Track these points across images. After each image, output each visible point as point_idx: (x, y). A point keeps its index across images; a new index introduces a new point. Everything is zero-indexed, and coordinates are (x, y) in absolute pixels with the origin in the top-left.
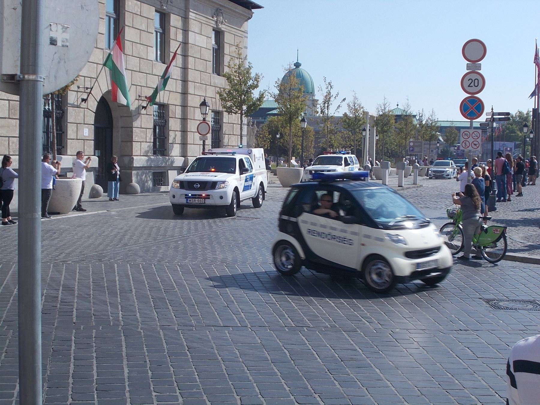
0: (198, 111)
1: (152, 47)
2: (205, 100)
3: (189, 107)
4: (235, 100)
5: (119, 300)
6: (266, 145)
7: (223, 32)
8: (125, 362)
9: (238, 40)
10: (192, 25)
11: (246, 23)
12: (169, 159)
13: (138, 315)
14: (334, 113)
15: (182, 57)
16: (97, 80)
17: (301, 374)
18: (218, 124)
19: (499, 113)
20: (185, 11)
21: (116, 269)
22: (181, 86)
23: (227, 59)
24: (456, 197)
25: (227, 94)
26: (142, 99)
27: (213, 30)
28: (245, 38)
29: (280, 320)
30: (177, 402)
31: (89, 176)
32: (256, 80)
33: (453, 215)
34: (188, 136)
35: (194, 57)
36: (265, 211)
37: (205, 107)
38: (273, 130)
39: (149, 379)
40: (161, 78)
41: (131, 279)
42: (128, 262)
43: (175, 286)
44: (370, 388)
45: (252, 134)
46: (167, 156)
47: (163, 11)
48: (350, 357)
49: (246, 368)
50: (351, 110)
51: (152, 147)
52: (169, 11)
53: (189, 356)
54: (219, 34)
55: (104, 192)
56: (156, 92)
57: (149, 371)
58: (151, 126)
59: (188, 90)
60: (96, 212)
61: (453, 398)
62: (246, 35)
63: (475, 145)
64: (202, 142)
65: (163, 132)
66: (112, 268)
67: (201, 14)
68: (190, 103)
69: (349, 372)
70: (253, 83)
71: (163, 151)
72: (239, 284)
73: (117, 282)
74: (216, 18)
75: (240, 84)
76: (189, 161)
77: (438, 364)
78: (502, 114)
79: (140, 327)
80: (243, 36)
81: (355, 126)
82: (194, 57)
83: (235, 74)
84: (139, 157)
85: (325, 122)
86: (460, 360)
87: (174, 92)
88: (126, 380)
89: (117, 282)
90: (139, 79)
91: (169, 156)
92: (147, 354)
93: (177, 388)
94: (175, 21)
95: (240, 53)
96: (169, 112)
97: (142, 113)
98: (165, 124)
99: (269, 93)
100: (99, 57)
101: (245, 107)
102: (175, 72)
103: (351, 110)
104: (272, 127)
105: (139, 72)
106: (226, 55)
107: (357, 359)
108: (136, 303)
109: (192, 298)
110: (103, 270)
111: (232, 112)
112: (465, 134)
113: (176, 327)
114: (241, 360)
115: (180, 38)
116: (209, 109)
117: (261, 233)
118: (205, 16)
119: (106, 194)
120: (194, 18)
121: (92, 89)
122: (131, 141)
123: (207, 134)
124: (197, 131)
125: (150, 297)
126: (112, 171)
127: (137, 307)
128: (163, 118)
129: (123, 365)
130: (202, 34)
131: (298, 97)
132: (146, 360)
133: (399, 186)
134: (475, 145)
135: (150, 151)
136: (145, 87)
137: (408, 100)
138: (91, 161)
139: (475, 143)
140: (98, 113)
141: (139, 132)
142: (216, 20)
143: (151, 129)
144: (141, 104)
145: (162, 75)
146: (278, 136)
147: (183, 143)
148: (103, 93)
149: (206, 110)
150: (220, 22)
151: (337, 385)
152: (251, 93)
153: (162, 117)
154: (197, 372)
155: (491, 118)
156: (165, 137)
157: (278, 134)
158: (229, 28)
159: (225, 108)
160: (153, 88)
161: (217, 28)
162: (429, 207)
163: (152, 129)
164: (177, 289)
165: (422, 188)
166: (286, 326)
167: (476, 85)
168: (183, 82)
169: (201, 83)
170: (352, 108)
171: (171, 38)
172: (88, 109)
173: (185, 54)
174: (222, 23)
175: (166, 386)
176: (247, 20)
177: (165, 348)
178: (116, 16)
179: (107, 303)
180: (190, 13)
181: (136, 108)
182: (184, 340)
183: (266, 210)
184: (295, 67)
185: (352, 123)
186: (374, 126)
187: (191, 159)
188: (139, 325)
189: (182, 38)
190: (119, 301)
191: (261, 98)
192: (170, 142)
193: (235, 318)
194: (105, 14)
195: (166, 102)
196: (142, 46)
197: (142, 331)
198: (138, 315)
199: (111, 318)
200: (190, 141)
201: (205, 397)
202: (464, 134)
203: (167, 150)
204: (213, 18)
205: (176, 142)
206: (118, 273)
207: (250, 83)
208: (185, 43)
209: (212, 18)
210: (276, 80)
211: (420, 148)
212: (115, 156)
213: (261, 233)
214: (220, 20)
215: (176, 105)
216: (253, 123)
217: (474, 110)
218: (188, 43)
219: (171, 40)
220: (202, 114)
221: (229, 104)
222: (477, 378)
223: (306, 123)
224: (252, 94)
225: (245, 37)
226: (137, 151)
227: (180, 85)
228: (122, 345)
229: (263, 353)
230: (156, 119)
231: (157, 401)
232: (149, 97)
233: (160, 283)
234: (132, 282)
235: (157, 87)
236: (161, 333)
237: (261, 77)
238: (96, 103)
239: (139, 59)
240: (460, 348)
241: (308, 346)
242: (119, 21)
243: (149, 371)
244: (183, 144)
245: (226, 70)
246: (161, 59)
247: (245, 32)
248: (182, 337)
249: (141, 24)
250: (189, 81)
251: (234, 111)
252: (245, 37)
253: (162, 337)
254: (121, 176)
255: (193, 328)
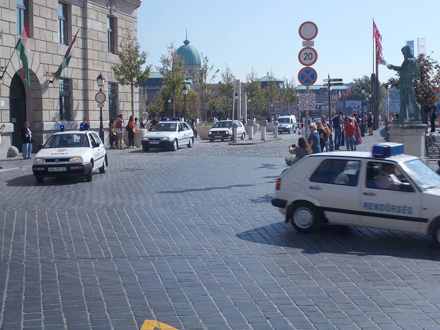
0: (96, 83)
1: (57, 32)
2: (101, 74)
3: (89, 80)
4: (126, 73)
5: (12, 240)
6: (161, 109)
7: (116, 18)
8: (6, 290)
9: (128, 24)
10: (90, 14)
11: (135, 10)
12: (73, 123)
13: (25, 252)
14: (210, 82)
15: (82, 40)
16: (10, 60)
17: (143, 294)
18: (115, 93)
19: (334, 79)
20: (84, 2)
21: (16, 215)
22: (82, 63)
23: (119, 40)
24: (291, 149)
25: (120, 69)
26: (49, 75)
27: (108, 17)
28: (135, 23)
29: (138, 252)
30: (40, 319)
31: (6, 139)
32: (143, 57)
33: (290, 162)
34: (89, 104)
35: (92, 39)
36: (149, 164)
37: (101, 80)
38: (166, 96)
39: (22, 302)
40: (64, 58)
41: (26, 223)
42: (26, 209)
43: (60, 228)
44: (195, 302)
45: (144, 100)
46: (71, 121)
47: (66, 3)
48: (186, 278)
49: (101, 291)
50: (225, 79)
51: (59, 114)
52: (70, 3)
53: (58, 283)
54: (113, 20)
55: (19, 152)
56: (61, 69)
57: (23, 296)
58: (58, 96)
59: (88, 66)
60: (11, 169)
61: (259, 307)
62: (136, 20)
63: (311, 106)
64: (99, 109)
65: (68, 101)
66: (13, 214)
67: (97, 4)
68: (90, 77)
69: (183, 290)
70: (141, 60)
71: (69, 117)
72: (276, 229)
73: (14, 226)
74: (110, 7)
75: (131, 61)
76: (90, 124)
77: (255, 281)
78: (336, 80)
79: (24, 261)
80: (133, 21)
81: (228, 92)
82: (92, 39)
83: (126, 52)
84: (48, 122)
85: (203, 89)
86: (273, 278)
87: (76, 68)
88: (4, 303)
89: (14, 226)
90: (47, 58)
91: (73, 121)
92: (24, 282)
93: (42, 308)
94: (75, 10)
95: (129, 35)
96: (72, 85)
97: (49, 86)
98: (70, 95)
99: (156, 67)
100: (12, 42)
101: (135, 79)
102: (76, 52)
103: (225, 79)
104: (165, 94)
105: (46, 53)
106: (119, 37)
107: (191, 280)
108: (26, 242)
109: (72, 236)
110: (5, 216)
111: (124, 83)
112: (303, 98)
113: (53, 261)
114: (99, 284)
115: (80, 24)
116: (105, 81)
117: (142, 181)
118: (101, 5)
119: (21, 154)
120: (91, 8)
121: (6, 68)
122: (41, 110)
123: (103, 102)
124: (95, 100)
125: (38, 237)
126: (26, 134)
127: (25, 246)
128: (68, 90)
129: (3, 292)
130: (98, 20)
131: (179, 70)
132: (23, 287)
133: (262, 140)
134: (311, 106)
135: (57, 117)
136: (51, 65)
137: (272, 69)
138: (5, 128)
139: (311, 104)
140: (12, 88)
141: (47, 102)
142: (110, 9)
143: (58, 99)
144: (48, 79)
145: (65, 55)
146: (169, 101)
147: (85, 110)
148: (16, 71)
149: (102, 82)
150: (113, 10)
151: (170, 300)
152: (139, 67)
153: (67, 89)
154: (61, 295)
155: (328, 84)
156: (69, 105)
157: (169, 100)
158: (121, 15)
159: (118, 80)
160: (58, 66)
161: (111, 15)
162: (282, 156)
163: (59, 99)
164: (61, 230)
165: (281, 140)
166: (141, 256)
167: (310, 58)
168: (83, 60)
169: (99, 60)
170: (226, 77)
171: (72, 24)
172: (3, 84)
173: (84, 37)
174: (115, 11)
175: (34, 307)
176: (135, 9)
177: (40, 277)
178: (26, 7)
179: (2, 243)
180: (88, 4)
181: (44, 83)
182: (57, 270)
183: (150, 163)
184: (185, 44)
185: (226, 89)
186: (244, 91)
187: (92, 123)
188: (24, 260)
189: (82, 24)
190: (12, 241)
191: (148, 71)
192: (74, 110)
193: (102, 251)
194: (16, 6)
195: (69, 77)
196: (48, 32)
197: (25, 265)
198: (25, 252)
199: (2, 255)
200: (91, 108)
201: (63, 315)
202: (302, 97)
203: (72, 116)
204: (107, 7)
205: (79, 110)
206: (16, 219)
207: (139, 59)
208: (84, 28)
209: (106, 7)
210: (161, 57)
211: (279, 108)
212: (27, 123)
213: (142, 181)
214: (113, 8)
215: (78, 79)
216: (144, 91)
217: (309, 78)
218: (87, 28)
219: (72, 26)
220: (98, 86)
221: (122, 77)
222: (282, 291)
223: (187, 90)
224: (140, 69)
225: (135, 22)
226: (46, 117)
227: (81, 62)
228: (6, 276)
229: (117, 278)
230: (62, 91)
231: (24, 319)
232: (55, 73)
233: (49, 225)
234: (26, 225)
235: (61, 65)
236: (40, 265)
237: (147, 54)
238: (11, 80)
239: (45, 42)
240: (276, 268)
241: (155, 272)
242: (28, 11)
243: (23, 296)
244: (85, 110)
245: (120, 49)
246: (64, 42)
247: (135, 17)
248: (56, 268)
249: (47, 14)
250: (89, 59)
251: (126, 83)
252: (135, 22)
253: (40, 269)
254: (33, 139)
255: (66, 261)
